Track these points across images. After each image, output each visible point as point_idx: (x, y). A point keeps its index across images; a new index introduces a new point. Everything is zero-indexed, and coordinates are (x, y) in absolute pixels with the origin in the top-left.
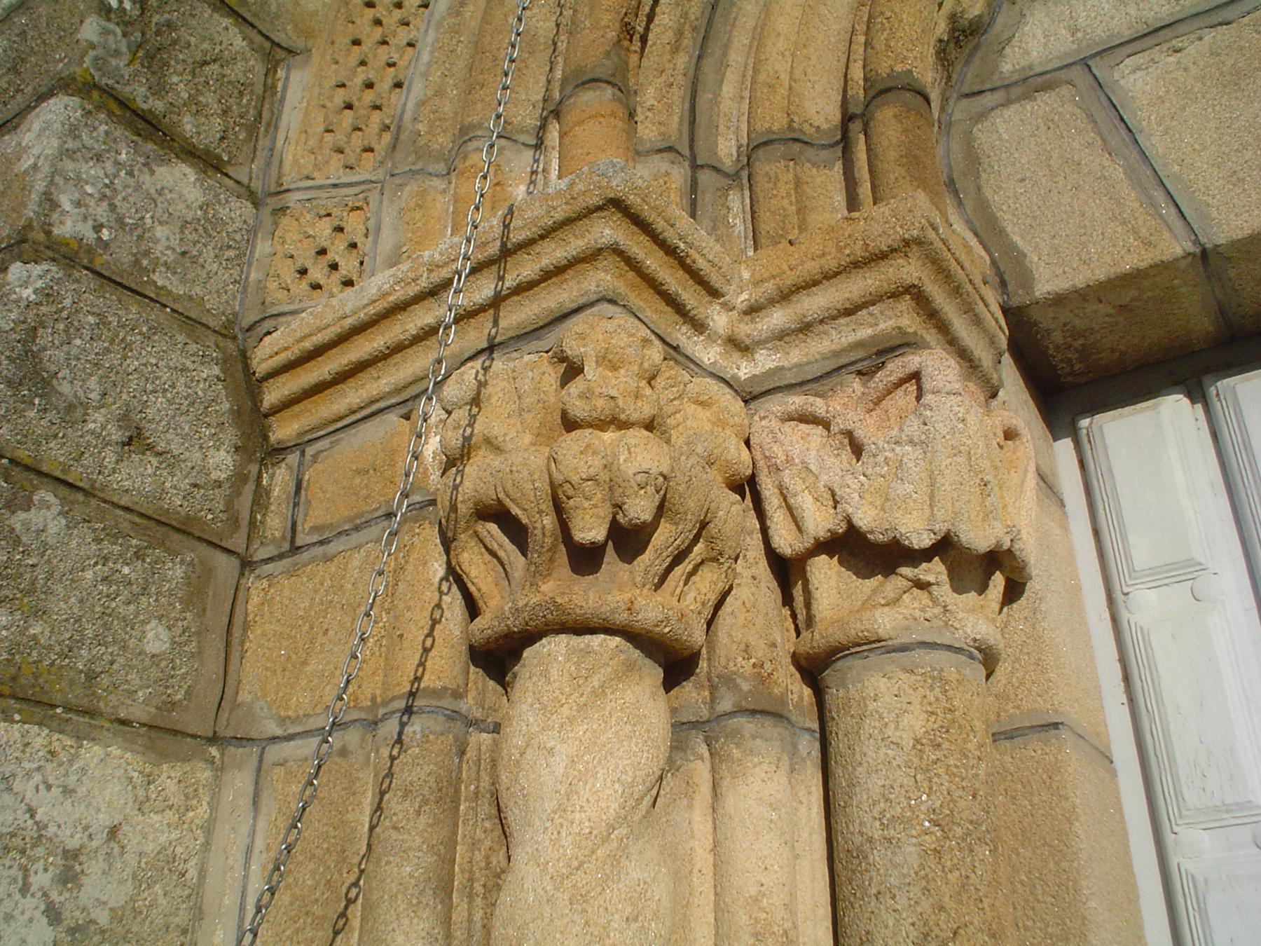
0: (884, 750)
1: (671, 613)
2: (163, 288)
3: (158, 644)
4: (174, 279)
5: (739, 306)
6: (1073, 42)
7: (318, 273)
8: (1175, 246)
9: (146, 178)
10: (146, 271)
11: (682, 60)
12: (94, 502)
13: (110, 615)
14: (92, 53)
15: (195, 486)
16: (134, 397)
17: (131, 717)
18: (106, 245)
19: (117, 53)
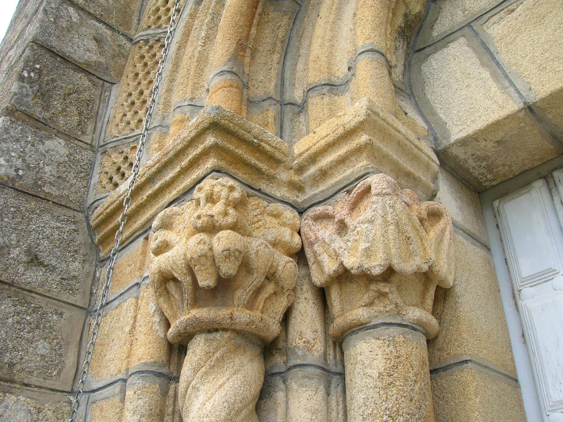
0: (364, 380)
1: (254, 318)
2: (48, 193)
3: (44, 350)
4: (54, 189)
5: (294, 167)
6: (464, 16)
7: (116, 178)
8: (513, 106)
9: (41, 147)
10: (40, 186)
11: (276, 57)
12: (13, 289)
13: (21, 338)
14: (15, 97)
15: (62, 279)
16: (34, 241)
17: (30, 383)
18: (21, 177)
19: (27, 95)
